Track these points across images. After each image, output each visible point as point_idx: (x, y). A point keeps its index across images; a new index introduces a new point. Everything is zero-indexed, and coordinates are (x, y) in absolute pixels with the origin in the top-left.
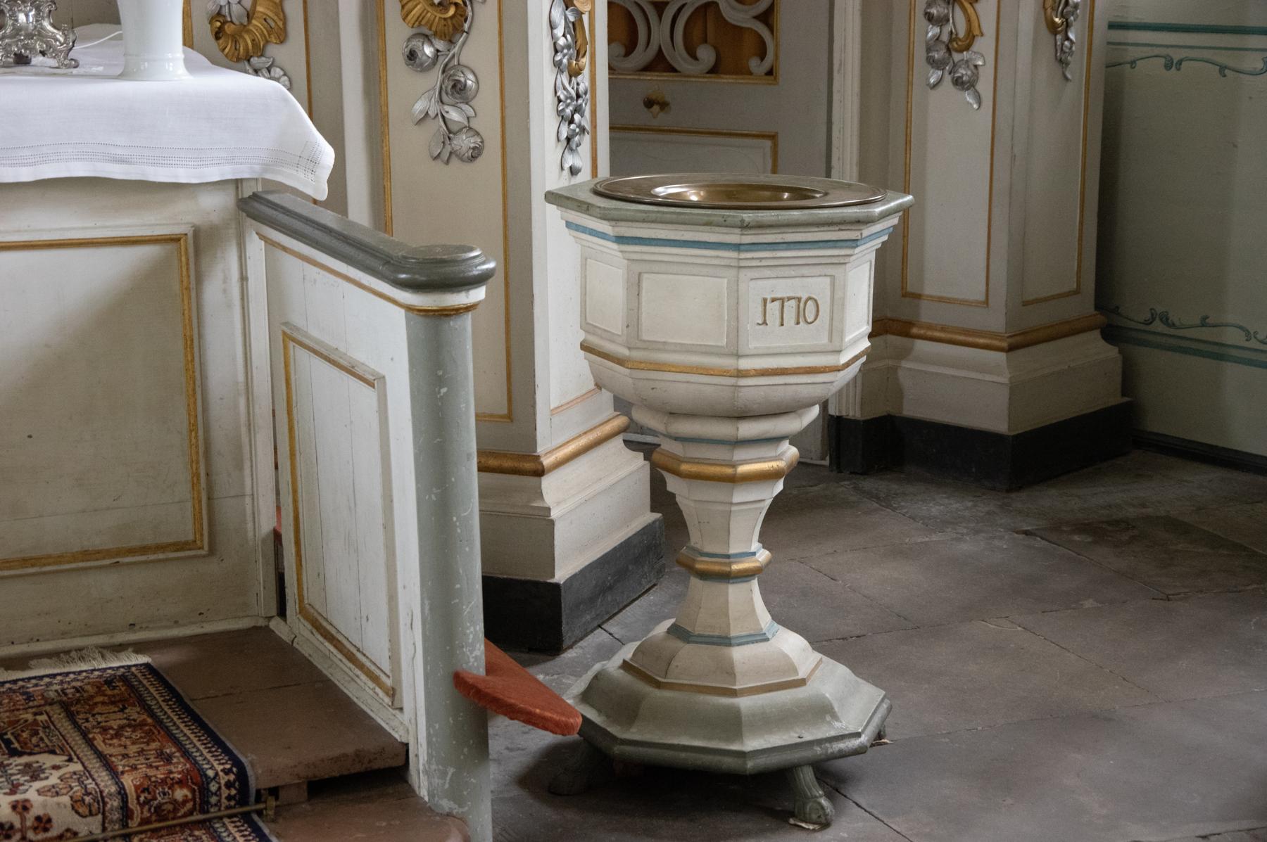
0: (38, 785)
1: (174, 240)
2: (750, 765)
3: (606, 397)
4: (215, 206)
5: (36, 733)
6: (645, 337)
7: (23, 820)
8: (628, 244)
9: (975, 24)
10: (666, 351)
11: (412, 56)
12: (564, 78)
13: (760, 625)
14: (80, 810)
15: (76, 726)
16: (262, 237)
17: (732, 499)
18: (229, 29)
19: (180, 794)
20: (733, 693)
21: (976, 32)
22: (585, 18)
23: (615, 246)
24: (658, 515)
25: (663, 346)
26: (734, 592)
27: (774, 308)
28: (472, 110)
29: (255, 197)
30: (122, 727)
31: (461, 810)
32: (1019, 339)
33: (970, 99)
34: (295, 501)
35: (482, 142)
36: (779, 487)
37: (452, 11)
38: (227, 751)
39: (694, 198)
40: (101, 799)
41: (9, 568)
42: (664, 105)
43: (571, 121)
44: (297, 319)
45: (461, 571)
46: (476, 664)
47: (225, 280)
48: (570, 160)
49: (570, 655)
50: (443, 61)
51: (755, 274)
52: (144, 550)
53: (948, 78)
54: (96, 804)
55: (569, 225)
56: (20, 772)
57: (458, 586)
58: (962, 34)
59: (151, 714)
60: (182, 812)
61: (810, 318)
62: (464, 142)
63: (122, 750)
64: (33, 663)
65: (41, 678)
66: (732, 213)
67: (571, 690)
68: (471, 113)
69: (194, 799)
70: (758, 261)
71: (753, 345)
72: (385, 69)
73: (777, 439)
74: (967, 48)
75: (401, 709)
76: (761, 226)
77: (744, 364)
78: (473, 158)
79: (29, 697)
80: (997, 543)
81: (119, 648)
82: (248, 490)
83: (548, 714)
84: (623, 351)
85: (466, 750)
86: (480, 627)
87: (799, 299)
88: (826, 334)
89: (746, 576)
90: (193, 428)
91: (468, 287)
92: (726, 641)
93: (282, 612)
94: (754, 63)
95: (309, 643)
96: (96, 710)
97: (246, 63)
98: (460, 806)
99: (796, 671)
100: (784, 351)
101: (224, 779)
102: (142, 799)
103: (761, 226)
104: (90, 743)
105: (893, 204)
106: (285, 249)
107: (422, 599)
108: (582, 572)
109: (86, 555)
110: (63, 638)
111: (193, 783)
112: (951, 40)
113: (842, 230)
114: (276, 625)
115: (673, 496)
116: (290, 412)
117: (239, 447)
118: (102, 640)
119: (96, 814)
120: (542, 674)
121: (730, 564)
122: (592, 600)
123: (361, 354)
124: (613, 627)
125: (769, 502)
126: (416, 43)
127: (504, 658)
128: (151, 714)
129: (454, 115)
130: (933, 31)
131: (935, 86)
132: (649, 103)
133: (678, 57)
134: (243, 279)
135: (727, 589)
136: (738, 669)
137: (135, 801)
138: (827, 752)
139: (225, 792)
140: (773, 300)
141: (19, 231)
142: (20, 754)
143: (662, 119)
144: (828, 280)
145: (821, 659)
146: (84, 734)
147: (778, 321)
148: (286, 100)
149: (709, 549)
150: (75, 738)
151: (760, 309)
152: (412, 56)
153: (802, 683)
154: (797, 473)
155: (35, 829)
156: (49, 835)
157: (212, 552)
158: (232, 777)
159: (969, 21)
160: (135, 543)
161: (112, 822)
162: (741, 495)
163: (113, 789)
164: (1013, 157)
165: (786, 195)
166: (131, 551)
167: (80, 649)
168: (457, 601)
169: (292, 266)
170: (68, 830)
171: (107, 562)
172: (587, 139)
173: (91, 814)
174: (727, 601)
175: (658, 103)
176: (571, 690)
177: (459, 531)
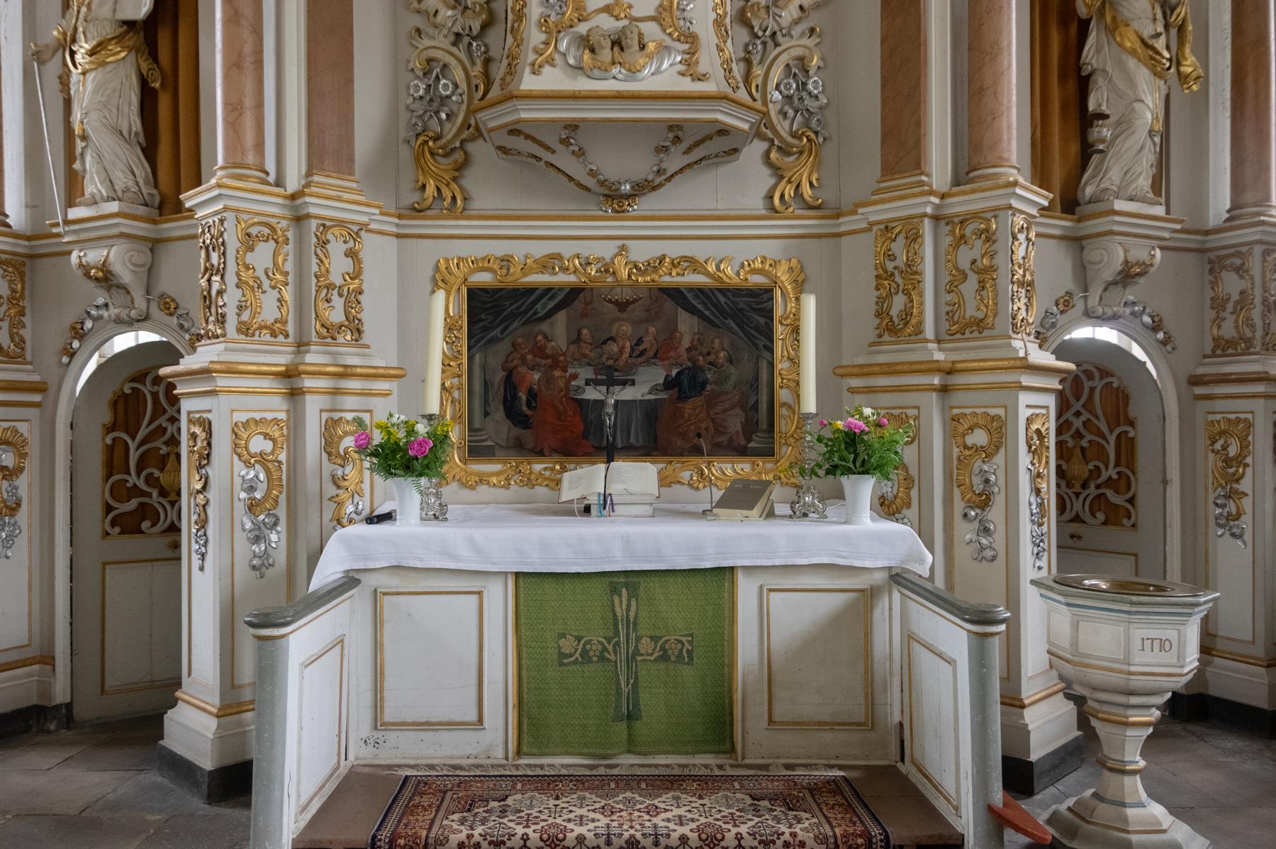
0: (800, 826)
1: (862, 591)
3: (1054, 673)
4: (879, 577)
5: (798, 801)
6: (1081, 651)
9: (1241, 508)
10: (1091, 658)
11: (965, 515)
12: (1036, 527)
15: (815, 800)
16: (899, 592)
18: (886, 502)
19: (860, 841)
20: (1128, 832)
21: (943, 346)
22: (1046, 501)
23: (1065, 607)
24: (1081, 733)
25: (1090, 656)
26: (1127, 780)
27: (1147, 643)
29: (897, 575)
30: (834, 804)
32: (1271, 662)
33: (1240, 543)
34: (911, 710)
36: (1151, 730)
37: (984, 497)
38: (880, 824)
39: (1104, 587)
40: (826, 838)
41: (789, 725)
42: (1079, 538)
43: (1039, 546)
44: (915, 630)
47: (883, 609)
48: (1038, 563)
49: (1038, 797)
50: (979, 518)
51: (1138, 626)
52: (844, 724)
53: (1227, 533)
55: (1041, 595)
56: (793, 818)
58: (1234, 513)
59: (847, 801)
61: (1167, 650)
62: (989, 553)
63: (834, 815)
64: (797, 768)
65: (800, 776)
66: (1126, 596)
67: (1042, 818)
68: (992, 540)
71: (1137, 660)
72: (953, 520)
73: (1151, 706)
74: (1237, 519)
75: (961, 817)
76: (1141, 604)
77: (1133, 669)
78: (992, 560)
79: (796, 784)
80: (1265, 766)
81: (832, 767)
82: (889, 702)
83: (1035, 832)
84: (1069, 656)
86: (1001, 784)
87: (1161, 640)
88: (1176, 657)
89: (1134, 772)
90: (866, 672)
92: (1123, 805)
93: (902, 760)
94: (1125, 521)
95: (915, 777)
96: (823, 795)
99: (1161, 825)
101: (879, 837)
103: (1141, 604)
104: (821, 810)
105: (1210, 597)
106: (910, 598)
107: (973, 766)
108: (1044, 757)
109: (820, 723)
112: (1228, 515)
114: (899, 765)
115: (1094, 728)
116: (909, 669)
117: (886, 682)
118: (824, 762)
120: (1024, 805)
121: (1125, 766)
122: (1049, 771)
123: (944, 649)
124: (1060, 785)
125: (1145, 737)
126: (966, 510)
127: (1011, 800)
128: (847, 801)
129: (984, 541)
130: (1218, 511)
131: (1220, 536)
132: (1072, 536)
133: (1087, 516)
134: (891, 609)
136: (1130, 820)
138: (664, 481)
139: (879, 844)
140: (1148, 639)
142: (793, 810)
143: (1078, 544)
144: (1176, 632)
145: (1174, 821)
146: (819, 805)
147: (1150, 650)
148: (913, 534)
149: (1113, 756)
150: (815, 806)
152: (965, 515)
153: (1164, 831)
154: (1157, 725)
157: (872, 728)
158: (883, 837)
159: (1238, 508)
160: (839, 721)
162: (1130, 732)
163: (831, 834)
164: (1265, 573)
165: (1152, 588)
166: (839, 724)
167: (815, 765)
169: (912, 605)
172: (1046, 553)
174: (1123, 785)
175: (1076, 536)
176: (1042, 818)
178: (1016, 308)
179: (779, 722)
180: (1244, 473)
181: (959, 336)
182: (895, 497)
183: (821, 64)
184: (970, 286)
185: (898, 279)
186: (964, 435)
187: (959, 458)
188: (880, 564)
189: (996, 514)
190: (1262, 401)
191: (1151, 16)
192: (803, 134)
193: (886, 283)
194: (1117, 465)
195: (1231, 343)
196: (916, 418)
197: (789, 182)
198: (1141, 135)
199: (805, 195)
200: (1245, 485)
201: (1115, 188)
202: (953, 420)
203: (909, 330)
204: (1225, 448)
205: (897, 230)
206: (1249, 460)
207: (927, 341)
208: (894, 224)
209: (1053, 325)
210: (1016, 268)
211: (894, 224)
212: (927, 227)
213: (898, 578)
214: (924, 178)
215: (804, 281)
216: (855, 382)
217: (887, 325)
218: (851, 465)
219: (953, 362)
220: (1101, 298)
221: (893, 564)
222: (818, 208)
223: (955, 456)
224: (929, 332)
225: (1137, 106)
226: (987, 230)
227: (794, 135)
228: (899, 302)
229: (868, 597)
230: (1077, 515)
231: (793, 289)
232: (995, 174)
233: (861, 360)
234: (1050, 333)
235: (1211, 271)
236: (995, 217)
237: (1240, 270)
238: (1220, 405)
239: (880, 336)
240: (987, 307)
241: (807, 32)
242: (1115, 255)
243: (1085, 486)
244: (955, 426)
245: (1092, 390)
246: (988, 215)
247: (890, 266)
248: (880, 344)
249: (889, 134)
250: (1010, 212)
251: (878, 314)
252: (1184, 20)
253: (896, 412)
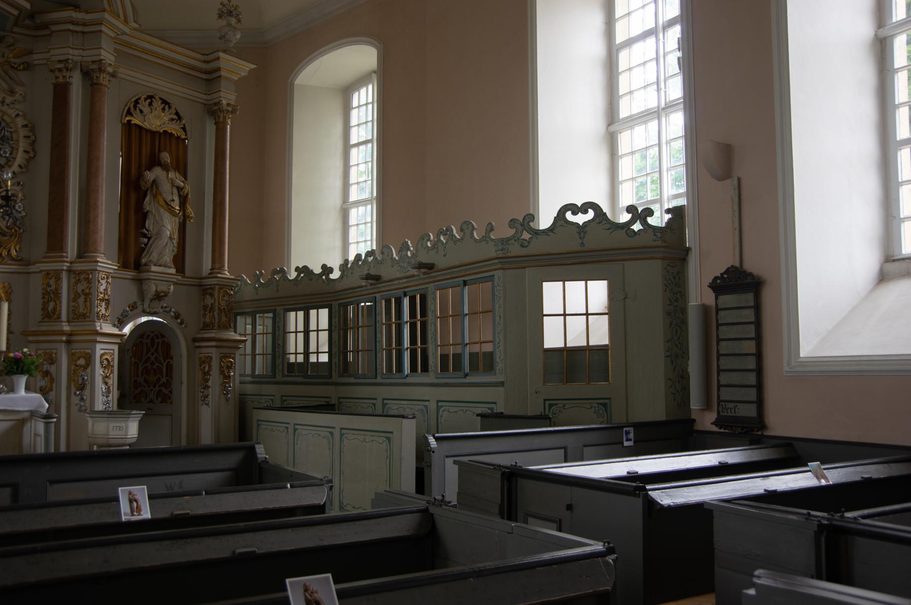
4: (26, 415)
22: (111, 388)
28: (460, 412)
62: (83, 408)
77: (110, 437)
129: (82, 404)
152: (75, 393)
168: (95, 447)
178: (99, 310)
180: (209, 378)
181: (76, 320)
182: (46, 387)
183: (23, 198)
184: (81, 300)
185: (52, 295)
186: (76, 361)
187: (74, 370)
188: (26, 409)
189: (87, 392)
190: (215, 349)
191: (171, 192)
192: (12, 228)
193: (47, 296)
194: (167, 376)
195: (208, 325)
196: (56, 354)
197: (5, 248)
198: (165, 240)
199: (13, 254)
200: (210, 384)
201: (155, 260)
202: (72, 354)
203: (55, 316)
204: (204, 368)
205: (52, 275)
206: (211, 373)
207: (62, 322)
208: (51, 272)
209: (126, 316)
210: (99, 294)
211: (51, 272)
212: (64, 276)
213: (33, 414)
214: (64, 254)
215: (10, 293)
216: (31, 338)
217: (46, 314)
218: (15, 371)
219: (72, 331)
220: (149, 305)
221: (32, 409)
222: (19, 260)
223: (73, 369)
224: (64, 317)
225: (163, 228)
226: (88, 278)
227: (8, 228)
228: (51, 305)
229: (23, 422)
230: (151, 399)
231: (5, 296)
232: (93, 256)
233: (35, 329)
234: (125, 319)
235: (203, 295)
236: (92, 273)
237: (212, 295)
238: (203, 350)
239: (43, 319)
240: (87, 309)
241: (16, 183)
242: (152, 289)
243: (155, 386)
244: (72, 357)
245: (158, 343)
246: (89, 272)
247: (49, 289)
248: (43, 322)
249: (50, 234)
250: (97, 272)
251: (43, 309)
252: (187, 194)
253: (48, 351)
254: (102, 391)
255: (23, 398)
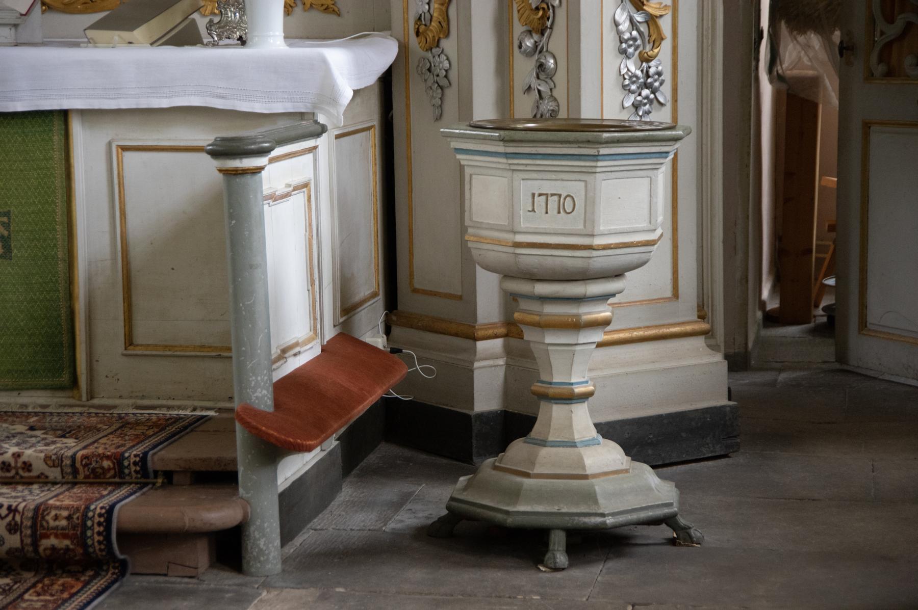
2: (510, 521)
7: (16, 462)
8: (491, 156)
13: (574, 436)
14: (48, 462)
17: (544, 340)
22: (665, 25)
28: (552, 83)
31: (247, 495)
35: (558, 106)
45: (245, 339)
46: (257, 401)
51: (526, 175)
54: (57, 461)
57: (244, 349)
60: (108, 475)
69: (114, 468)
70: (524, 166)
85: (249, 456)
87: (560, 196)
88: (582, 222)
91: (241, 156)
97: (430, 52)
98: (247, 493)
100: (548, 231)
102: (84, 462)
110: (188, 400)
111: (114, 458)
113: (581, 147)
119: (57, 467)
135: (552, 407)
137: (80, 463)
140: (540, 195)
141: (169, 140)
144: (583, 184)
151: (530, 200)
155: (23, 469)
156: (31, 474)
161: (67, 473)
168: (243, 358)
170: (42, 474)
171: (214, 354)
173: (54, 466)
174: (551, 417)
177: (244, 313)
179: (142, 345)
189: (557, 41)
254: (619, 33)
255: (274, 66)
